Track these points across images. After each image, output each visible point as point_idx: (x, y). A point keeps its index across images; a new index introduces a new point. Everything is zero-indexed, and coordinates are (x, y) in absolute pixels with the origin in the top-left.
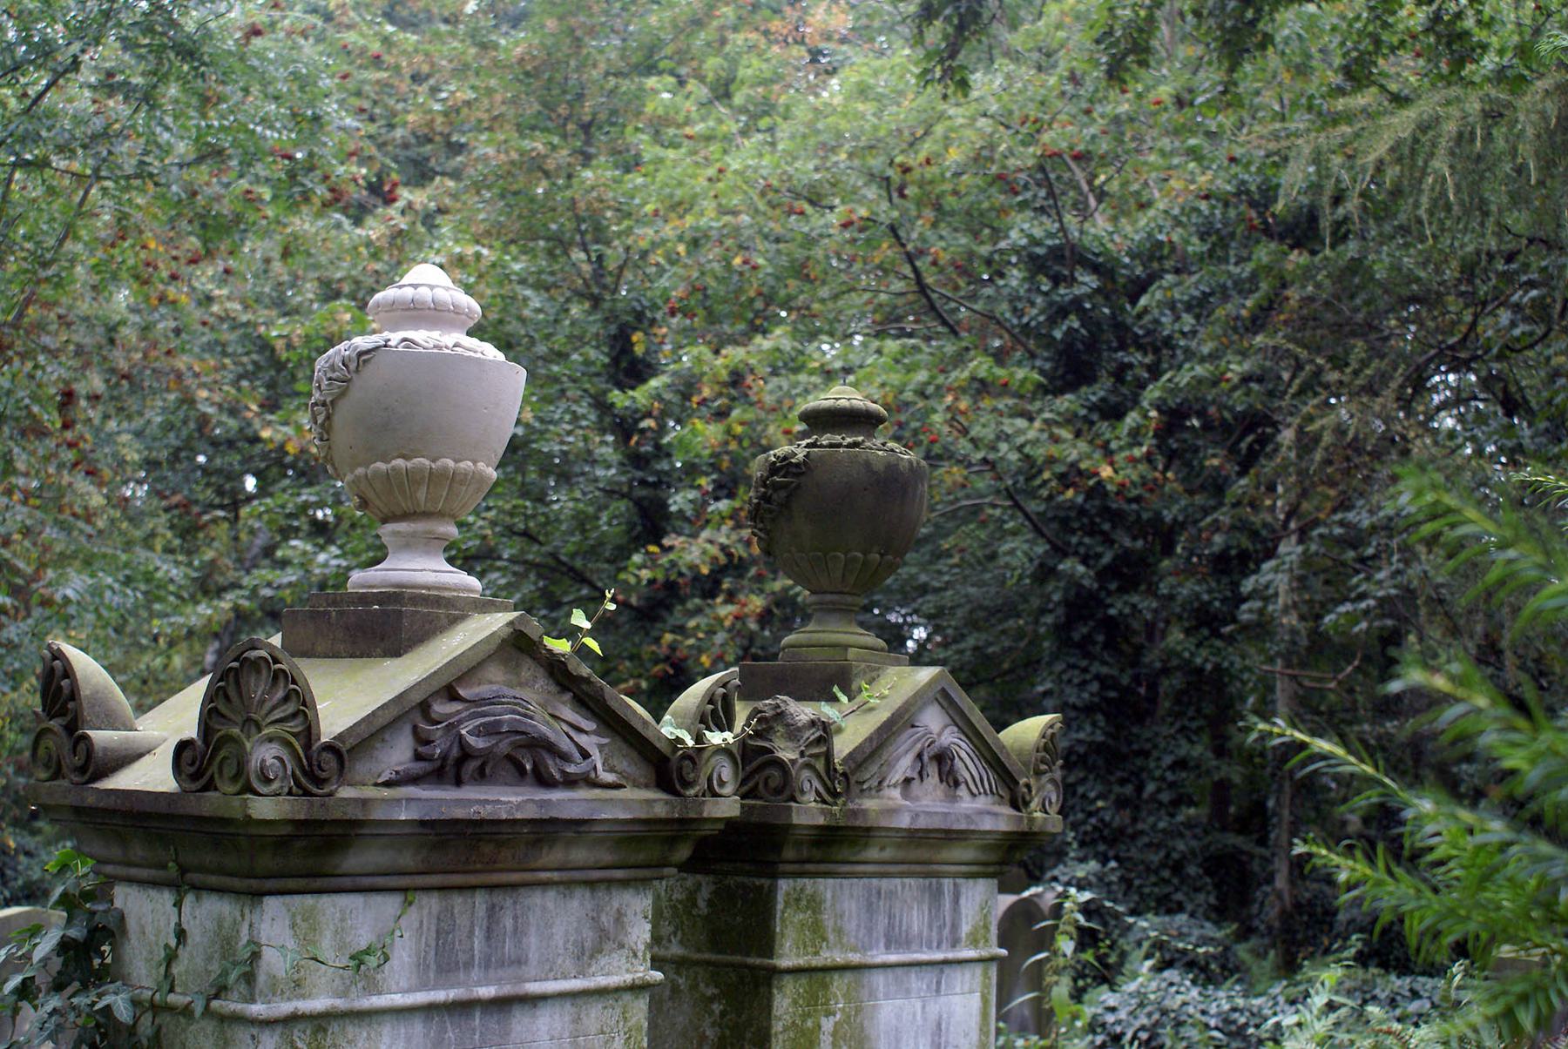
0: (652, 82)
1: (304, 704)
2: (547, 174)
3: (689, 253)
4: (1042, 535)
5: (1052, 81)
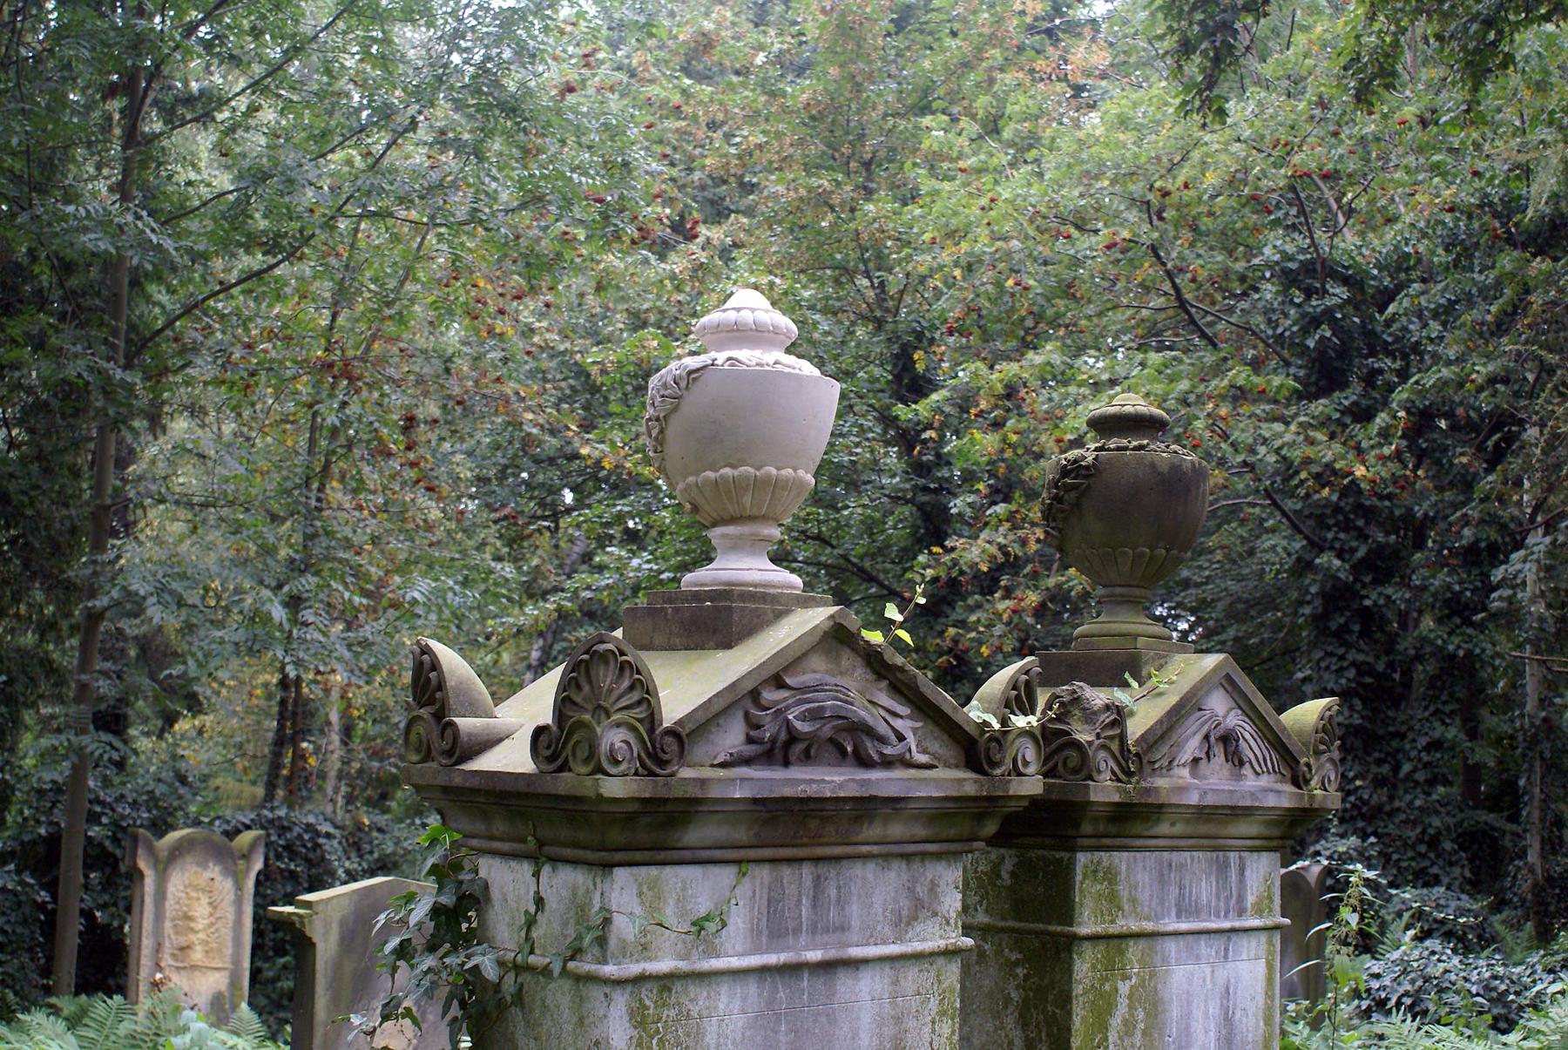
0: (927, 121)
1: (648, 692)
2: (832, 208)
3: (964, 278)
4: (1300, 532)
5: (1302, 106)
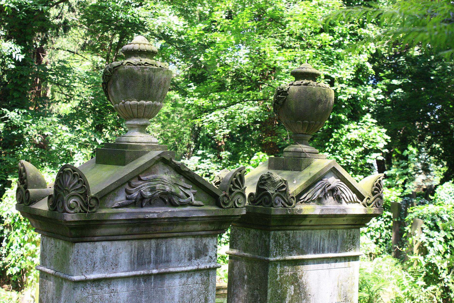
1: (84, 184)
